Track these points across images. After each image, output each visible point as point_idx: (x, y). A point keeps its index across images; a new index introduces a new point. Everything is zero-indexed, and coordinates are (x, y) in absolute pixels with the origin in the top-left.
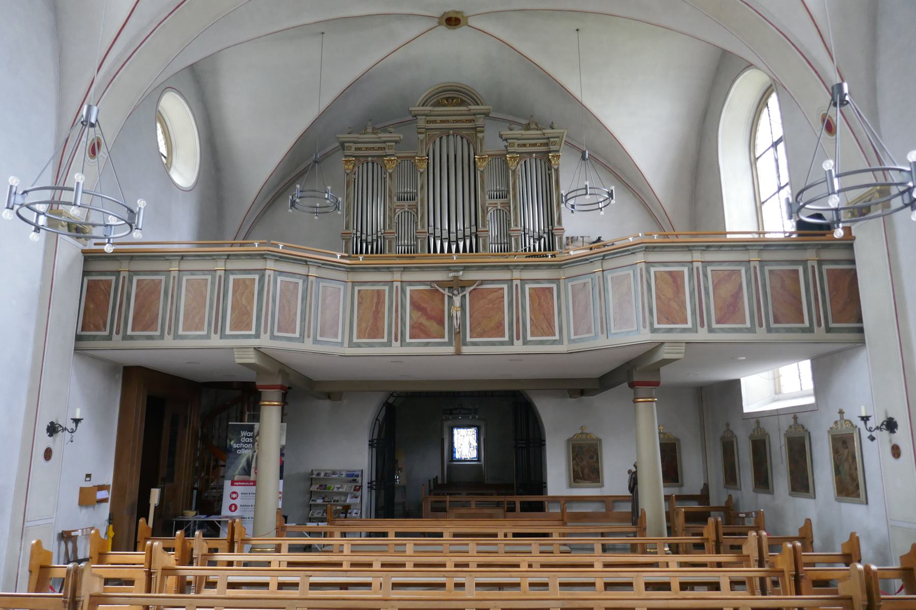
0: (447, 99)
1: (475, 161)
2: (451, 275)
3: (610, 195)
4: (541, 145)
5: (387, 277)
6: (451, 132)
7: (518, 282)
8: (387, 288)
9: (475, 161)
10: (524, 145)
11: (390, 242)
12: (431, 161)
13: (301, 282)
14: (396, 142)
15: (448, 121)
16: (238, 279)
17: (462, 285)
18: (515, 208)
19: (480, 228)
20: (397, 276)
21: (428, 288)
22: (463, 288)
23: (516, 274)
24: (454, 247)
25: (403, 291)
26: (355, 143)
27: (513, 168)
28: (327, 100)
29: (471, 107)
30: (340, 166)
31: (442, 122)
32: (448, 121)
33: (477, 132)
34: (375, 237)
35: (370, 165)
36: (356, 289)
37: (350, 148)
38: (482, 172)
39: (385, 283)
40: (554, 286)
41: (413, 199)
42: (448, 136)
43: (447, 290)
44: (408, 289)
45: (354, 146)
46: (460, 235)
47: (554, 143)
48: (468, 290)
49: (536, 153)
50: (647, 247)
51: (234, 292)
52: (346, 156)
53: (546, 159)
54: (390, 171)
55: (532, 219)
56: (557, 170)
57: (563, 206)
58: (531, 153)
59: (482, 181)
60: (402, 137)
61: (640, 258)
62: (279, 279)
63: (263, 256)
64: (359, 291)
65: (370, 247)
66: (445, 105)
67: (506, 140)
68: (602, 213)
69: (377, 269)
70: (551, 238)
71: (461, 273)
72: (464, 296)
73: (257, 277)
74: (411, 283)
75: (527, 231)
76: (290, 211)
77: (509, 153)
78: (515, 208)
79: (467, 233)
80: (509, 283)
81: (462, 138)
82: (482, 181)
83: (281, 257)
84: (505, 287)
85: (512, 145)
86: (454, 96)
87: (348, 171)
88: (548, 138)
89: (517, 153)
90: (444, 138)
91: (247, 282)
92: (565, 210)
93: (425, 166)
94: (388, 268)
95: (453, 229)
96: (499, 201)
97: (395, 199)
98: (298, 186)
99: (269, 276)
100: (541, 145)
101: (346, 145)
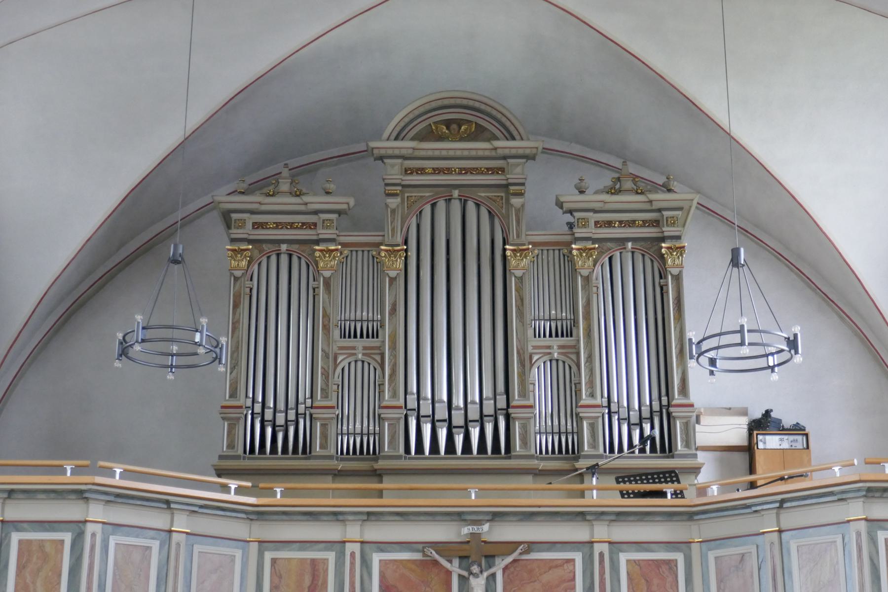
0: (448, 123)
1: (504, 257)
2: (466, 530)
3: (792, 344)
4: (645, 223)
5: (332, 532)
6: (456, 193)
7: (605, 548)
8: (331, 556)
9: (504, 257)
10: (609, 224)
11: (323, 426)
12: (413, 254)
13: (155, 545)
14: (339, 213)
15: (448, 171)
16: (29, 542)
17: (489, 553)
18: (590, 358)
19: (516, 400)
20: (353, 531)
21: (417, 556)
22: (490, 558)
23: (602, 531)
24: (459, 440)
25: (366, 563)
26: (252, 212)
27: (585, 273)
28: (196, 118)
29: (497, 144)
30: (214, 253)
31: (437, 171)
32: (448, 171)
33: (509, 194)
34: (292, 415)
35: (284, 259)
36: (268, 556)
37: (242, 224)
38: (520, 280)
39: (328, 544)
40: (680, 557)
41: (375, 335)
42: (448, 201)
43: (456, 562)
44: (376, 559)
45: (251, 219)
46: (474, 414)
47: (673, 222)
48: (501, 563)
49: (634, 240)
50: (869, 490)
51: (20, 568)
52: (233, 241)
53: (656, 251)
54: (327, 274)
55: (624, 376)
56: (678, 279)
57: (692, 364)
58: (623, 241)
59: (521, 300)
60: (352, 202)
61: (856, 510)
62: (113, 541)
63: (81, 495)
64: (274, 561)
65: (280, 436)
66: (441, 138)
67: (571, 212)
68: (775, 377)
69: (312, 516)
70: (666, 422)
71: (486, 527)
72: (493, 575)
73: (67, 538)
74: (382, 546)
75: (614, 408)
76: (117, 364)
77: (577, 240)
78: (590, 358)
79: (489, 409)
80: (586, 549)
81: (478, 206)
82: (521, 300)
83: (118, 496)
84: (578, 557)
85: (585, 223)
86: (461, 119)
87: (238, 273)
88: (659, 210)
89: (594, 241)
90: (441, 205)
91: (48, 548)
92: (696, 371)
93: (400, 264)
94: (335, 514)
95: (458, 401)
96: (556, 342)
97: (337, 333)
98: (139, 318)
99: (93, 535)
100: (645, 223)
101: (234, 216)
